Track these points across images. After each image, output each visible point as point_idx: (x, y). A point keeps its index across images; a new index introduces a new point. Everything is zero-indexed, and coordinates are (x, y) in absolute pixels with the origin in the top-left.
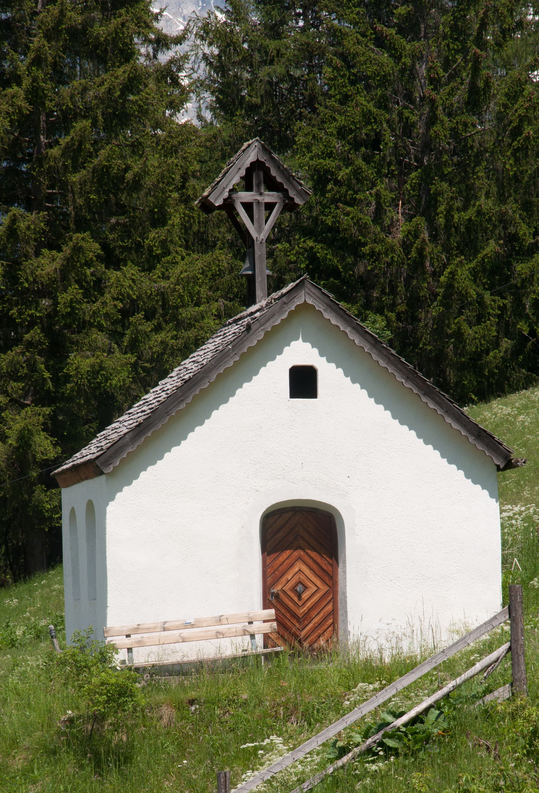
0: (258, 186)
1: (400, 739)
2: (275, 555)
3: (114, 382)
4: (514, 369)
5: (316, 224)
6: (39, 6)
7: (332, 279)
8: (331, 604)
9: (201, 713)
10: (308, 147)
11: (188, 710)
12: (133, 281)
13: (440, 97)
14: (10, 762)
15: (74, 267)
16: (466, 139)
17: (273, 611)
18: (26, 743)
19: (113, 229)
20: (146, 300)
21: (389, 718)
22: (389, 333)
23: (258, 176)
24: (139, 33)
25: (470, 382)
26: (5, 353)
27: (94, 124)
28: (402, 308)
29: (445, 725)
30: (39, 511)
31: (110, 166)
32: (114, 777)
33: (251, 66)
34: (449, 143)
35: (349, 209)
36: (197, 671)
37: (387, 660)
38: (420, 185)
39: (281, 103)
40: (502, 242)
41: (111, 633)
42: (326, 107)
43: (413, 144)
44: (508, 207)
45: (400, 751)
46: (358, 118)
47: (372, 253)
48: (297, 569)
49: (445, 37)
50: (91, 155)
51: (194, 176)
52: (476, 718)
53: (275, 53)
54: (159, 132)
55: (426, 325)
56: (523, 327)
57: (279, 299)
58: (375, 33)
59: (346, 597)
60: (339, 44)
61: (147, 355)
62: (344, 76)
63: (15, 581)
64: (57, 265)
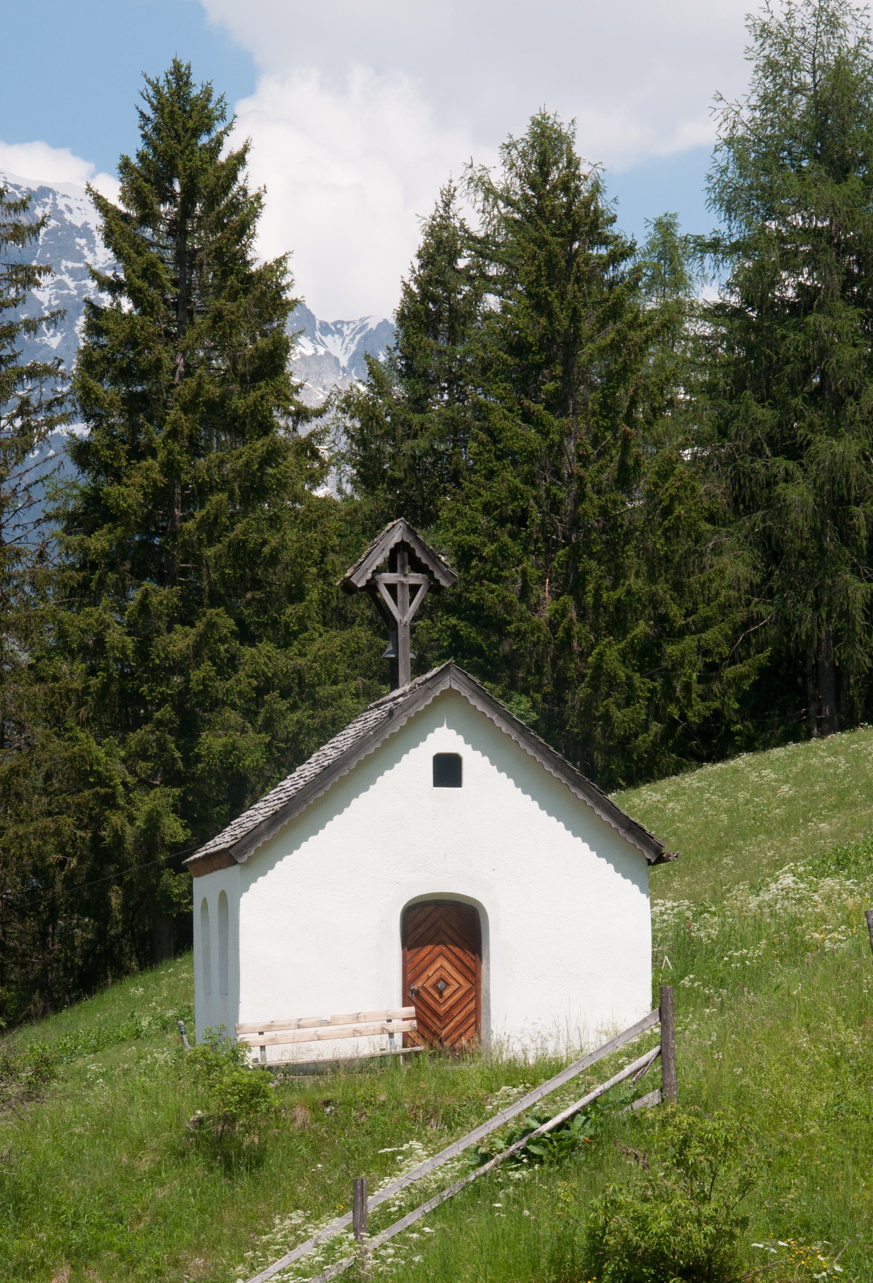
0: (403, 567)
1: (545, 1145)
2: (416, 950)
3: (247, 763)
4: (663, 754)
5: (460, 601)
6: (177, 379)
7: (475, 658)
8: (474, 1002)
9: (336, 1115)
10: (452, 523)
11: (323, 1111)
12: (269, 658)
13: (589, 474)
14: (137, 1164)
15: (207, 643)
16: (615, 517)
17: (412, 1009)
18: (154, 1144)
19: (248, 604)
20: (281, 677)
21: (534, 1124)
22: (534, 714)
23: (402, 557)
24: (279, 406)
25: (618, 767)
26: (134, 731)
27: (231, 497)
28: (548, 689)
29: (592, 1132)
30: (166, 897)
31: (247, 540)
32: (245, 1181)
33: (394, 440)
34: (598, 521)
35: (494, 586)
36: (333, 1071)
37: (531, 1061)
38: (567, 562)
39: (425, 478)
40: (652, 622)
41: (243, 1030)
42: (471, 482)
43: (561, 521)
44: (658, 587)
45: (545, 1158)
46: (504, 494)
47: (518, 632)
48: (438, 965)
49: (594, 414)
50: (226, 529)
51: (333, 551)
52: (624, 1124)
53: (418, 427)
54: (298, 506)
55: (573, 707)
56: (673, 710)
57: (422, 684)
58: (522, 409)
59: (489, 995)
60: (485, 418)
61: (282, 734)
62: (490, 451)
63: (141, 969)
64: (190, 641)
